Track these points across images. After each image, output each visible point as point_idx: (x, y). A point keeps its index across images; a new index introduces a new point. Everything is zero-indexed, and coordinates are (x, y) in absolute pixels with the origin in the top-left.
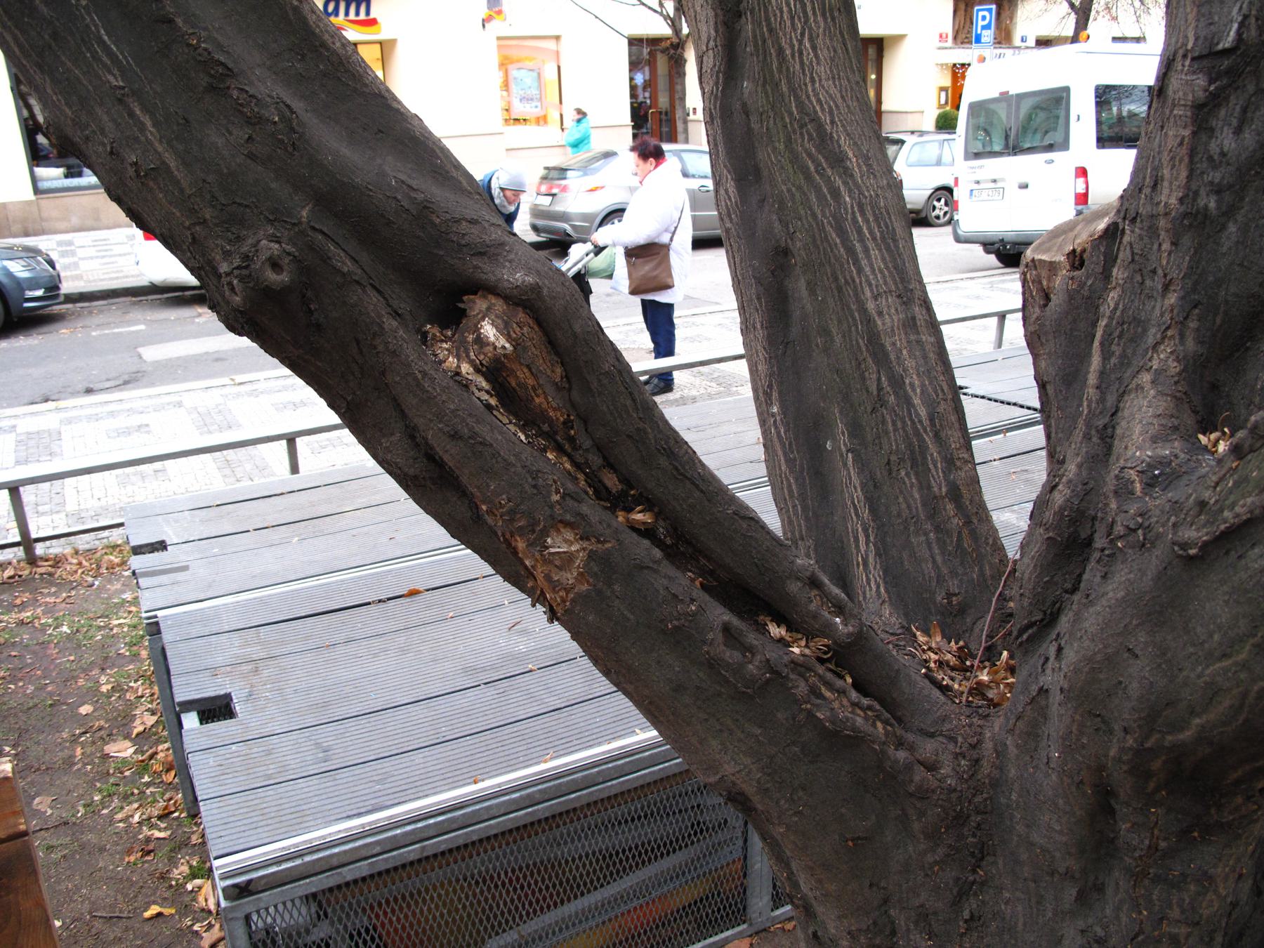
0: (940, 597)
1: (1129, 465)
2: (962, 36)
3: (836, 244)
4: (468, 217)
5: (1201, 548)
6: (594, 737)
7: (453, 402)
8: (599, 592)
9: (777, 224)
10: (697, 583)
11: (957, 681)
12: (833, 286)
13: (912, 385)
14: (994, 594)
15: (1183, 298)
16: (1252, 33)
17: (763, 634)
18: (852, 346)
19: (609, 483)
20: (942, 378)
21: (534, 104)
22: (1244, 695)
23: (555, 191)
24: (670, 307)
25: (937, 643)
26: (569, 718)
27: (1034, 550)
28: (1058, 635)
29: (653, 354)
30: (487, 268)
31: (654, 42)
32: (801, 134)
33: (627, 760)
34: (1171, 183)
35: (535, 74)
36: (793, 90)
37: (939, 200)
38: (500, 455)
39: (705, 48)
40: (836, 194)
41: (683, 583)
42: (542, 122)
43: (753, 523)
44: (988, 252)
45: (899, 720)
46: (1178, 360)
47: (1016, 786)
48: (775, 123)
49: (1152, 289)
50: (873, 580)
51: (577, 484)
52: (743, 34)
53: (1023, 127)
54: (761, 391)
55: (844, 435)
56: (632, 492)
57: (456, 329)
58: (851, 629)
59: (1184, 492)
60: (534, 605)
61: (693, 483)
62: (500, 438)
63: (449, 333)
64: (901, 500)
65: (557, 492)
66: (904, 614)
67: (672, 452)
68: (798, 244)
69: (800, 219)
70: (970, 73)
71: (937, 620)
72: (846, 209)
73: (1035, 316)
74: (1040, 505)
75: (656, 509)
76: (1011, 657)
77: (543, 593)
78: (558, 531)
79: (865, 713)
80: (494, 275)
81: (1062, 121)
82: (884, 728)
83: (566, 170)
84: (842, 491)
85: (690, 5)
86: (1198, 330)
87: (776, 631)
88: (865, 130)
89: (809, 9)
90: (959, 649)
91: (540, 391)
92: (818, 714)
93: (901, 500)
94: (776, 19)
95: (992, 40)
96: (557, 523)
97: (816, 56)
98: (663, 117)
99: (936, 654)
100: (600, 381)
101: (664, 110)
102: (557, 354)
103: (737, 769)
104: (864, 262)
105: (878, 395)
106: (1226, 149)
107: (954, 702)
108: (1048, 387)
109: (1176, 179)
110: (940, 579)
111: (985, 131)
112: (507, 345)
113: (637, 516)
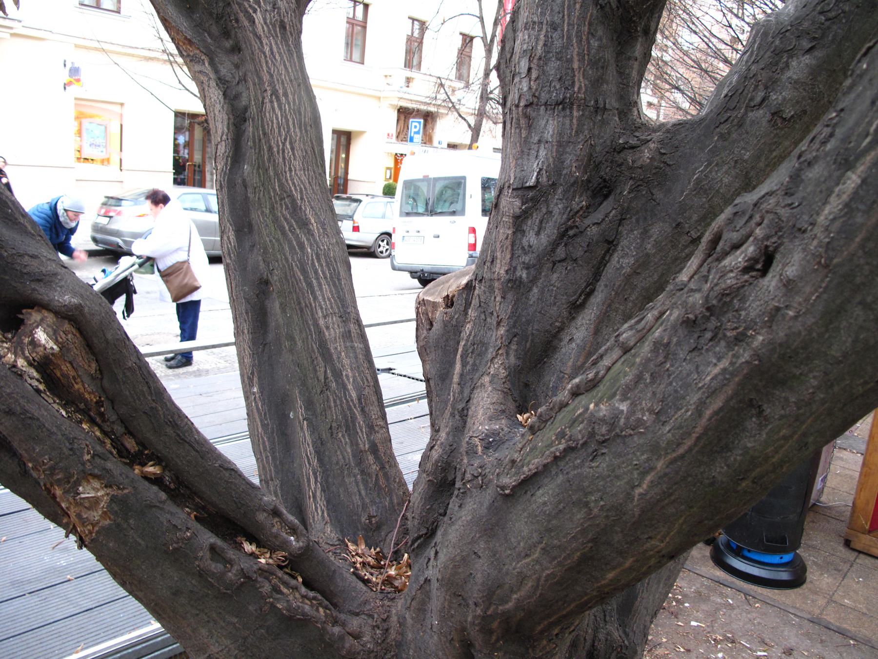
0: (364, 519)
1: (475, 435)
2: (401, 136)
3: (300, 280)
4: (30, 253)
5: (512, 490)
6: (118, 629)
7: (9, 387)
8: (118, 525)
9: (261, 263)
10: (192, 516)
11: (375, 575)
12: (297, 307)
13: (347, 376)
14: (399, 515)
15: (508, 331)
16: (544, 179)
17: (240, 550)
18: (308, 348)
19: (129, 446)
20: (367, 371)
21: (101, 149)
22: (539, 580)
23: (111, 214)
24: (197, 303)
25: (362, 550)
26: (98, 616)
27: (420, 489)
28: (436, 543)
29: (179, 338)
30: (42, 290)
31: (193, 116)
32: (281, 204)
33: (144, 645)
34: (501, 261)
35: (103, 128)
36: (277, 174)
37: (383, 241)
38: (44, 426)
39: (220, 140)
40: (302, 246)
41: (182, 517)
42: (106, 163)
43: (233, 473)
44: (413, 277)
45: (335, 605)
46: (505, 369)
47: (412, 646)
48: (264, 195)
49: (491, 324)
50: (319, 508)
51: (105, 447)
52: (247, 133)
53: (437, 199)
54: (246, 376)
55: (301, 409)
56: (146, 452)
57: (15, 333)
58: (301, 544)
59: (506, 453)
60: (67, 536)
61: (191, 446)
62: (45, 413)
63: (10, 336)
64: (339, 453)
65: (89, 453)
66: (341, 531)
67: (176, 424)
68: (275, 278)
69: (277, 261)
70: (405, 160)
71: (362, 534)
72: (308, 257)
73: (423, 336)
74: (425, 458)
75: (164, 464)
76: (409, 558)
77: (74, 527)
78: (88, 482)
79: (311, 603)
80: (48, 296)
81: (461, 197)
82: (325, 612)
83: (122, 200)
84: (300, 447)
85: (211, 109)
86: (516, 350)
87: (249, 547)
88: (323, 205)
89: (291, 123)
90: (376, 553)
91: (79, 380)
92: (278, 605)
93: (339, 453)
94: (268, 127)
95: (420, 141)
96: (87, 476)
97: (294, 154)
98: (197, 169)
99: (361, 557)
100: (124, 373)
101: (197, 164)
102: (93, 354)
103: (220, 649)
104: (318, 293)
105: (325, 382)
106: (531, 244)
107: (372, 590)
108: (431, 382)
109: (504, 259)
110: (364, 506)
111: (414, 199)
112: (55, 347)
113: (150, 469)
